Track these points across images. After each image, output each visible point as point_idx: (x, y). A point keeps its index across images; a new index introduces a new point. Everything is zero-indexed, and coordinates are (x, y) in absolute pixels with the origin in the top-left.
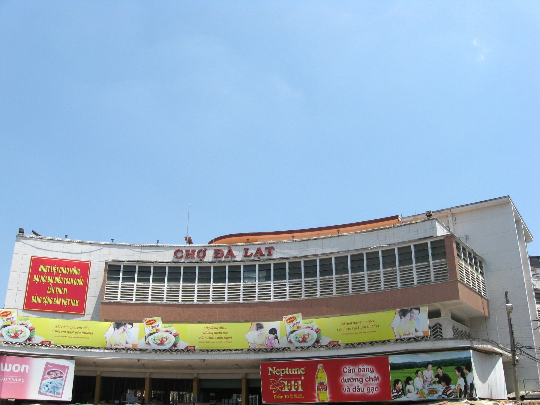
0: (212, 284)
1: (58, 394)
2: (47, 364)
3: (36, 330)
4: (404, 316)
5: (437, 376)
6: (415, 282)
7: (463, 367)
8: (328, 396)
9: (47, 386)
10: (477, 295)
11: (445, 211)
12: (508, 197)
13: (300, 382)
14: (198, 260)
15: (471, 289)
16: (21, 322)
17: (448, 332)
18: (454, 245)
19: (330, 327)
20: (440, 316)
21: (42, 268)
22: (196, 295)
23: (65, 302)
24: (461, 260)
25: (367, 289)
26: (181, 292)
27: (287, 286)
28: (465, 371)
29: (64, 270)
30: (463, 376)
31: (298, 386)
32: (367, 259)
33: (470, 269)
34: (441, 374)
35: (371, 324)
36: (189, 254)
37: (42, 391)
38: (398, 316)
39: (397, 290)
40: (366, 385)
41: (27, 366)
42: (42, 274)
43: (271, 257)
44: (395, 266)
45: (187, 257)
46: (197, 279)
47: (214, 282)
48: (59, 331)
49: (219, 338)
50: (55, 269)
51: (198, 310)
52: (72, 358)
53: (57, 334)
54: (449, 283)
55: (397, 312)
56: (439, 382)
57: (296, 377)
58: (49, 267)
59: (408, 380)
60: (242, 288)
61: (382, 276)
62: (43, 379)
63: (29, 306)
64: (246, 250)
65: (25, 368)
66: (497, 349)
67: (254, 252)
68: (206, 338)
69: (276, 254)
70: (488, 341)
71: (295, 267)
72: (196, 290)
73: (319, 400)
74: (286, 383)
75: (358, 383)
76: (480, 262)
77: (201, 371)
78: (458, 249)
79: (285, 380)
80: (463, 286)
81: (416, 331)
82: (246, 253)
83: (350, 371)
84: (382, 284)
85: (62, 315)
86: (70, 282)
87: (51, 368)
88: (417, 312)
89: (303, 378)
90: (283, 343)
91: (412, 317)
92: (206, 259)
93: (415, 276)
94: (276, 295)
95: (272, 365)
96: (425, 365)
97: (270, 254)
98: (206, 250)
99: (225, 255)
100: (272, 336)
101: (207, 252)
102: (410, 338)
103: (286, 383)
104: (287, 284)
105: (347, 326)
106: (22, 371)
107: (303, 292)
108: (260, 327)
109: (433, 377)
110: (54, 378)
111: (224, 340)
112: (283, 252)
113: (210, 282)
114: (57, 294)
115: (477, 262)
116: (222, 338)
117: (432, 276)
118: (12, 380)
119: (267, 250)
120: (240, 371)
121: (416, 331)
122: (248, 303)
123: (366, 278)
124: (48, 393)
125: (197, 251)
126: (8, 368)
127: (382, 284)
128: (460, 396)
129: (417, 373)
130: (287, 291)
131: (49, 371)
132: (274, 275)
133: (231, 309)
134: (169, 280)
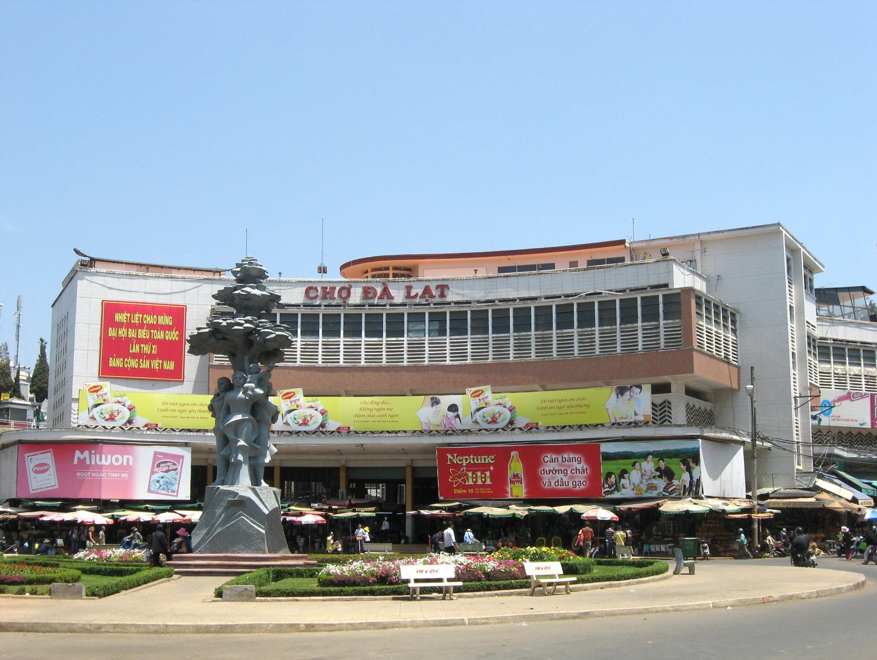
0: (363, 338)
1: (173, 492)
2: (156, 453)
3: (137, 409)
4: (622, 395)
5: (658, 469)
6: (640, 347)
7: (690, 460)
8: (524, 491)
9: (158, 482)
10: (721, 364)
11: (692, 238)
12: (779, 224)
13: (488, 473)
14: (340, 301)
15: (713, 357)
16: (116, 399)
17: (679, 414)
18: (693, 302)
19: (528, 405)
20: (670, 392)
21: (120, 317)
22: (342, 353)
23: (156, 364)
24: (702, 319)
25: (576, 352)
26: (320, 350)
27: (469, 344)
28: (691, 464)
29: (150, 319)
30: (689, 469)
31: (485, 477)
32: (578, 312)
33: (714, 329)
34: (663, 467)
35: (580, 403)
36: (327, 293)
37: (152, 489)
38: (614, 395)
39: (616, 356)
40: (571, 478)
41: (130, 457)
42: (120, 325)
43: (444, 300)
44: (616, 324)
45: (324, 297)
46: (342, 332)
47: (366, 336)
48: (166, 410)
49: (381, 416)
50: (137, 318)
51: (346, 374)
52: (186, 445)
53: (164, 413)
54: (682, 350)
55: (614, 390)
56: (660, 477)
57: (484, 467)
58: (129, 315)
59: (623, 473)
60: (405, 345)
61: (597, 336)
62: (153, 473)
63: (106, 372)
64: (409, 288)
65: (128, 460)
66: (735, 437)
67: (420, 291)
68: (363, 416)
69: (451, 297)
70: (723, 429)
71: (480, 318)
72: (342, 347)
73: (512, 495)
74: (470, 474)
75: (562, 476)
76: (733, 315)
77: (352, 457)
78: (698, 305)
79: (469, 471)
80: (700, 355)
81: (636, 414)
82: (409, 293)
83: (552, 461)
84: (597, 347)
85: (153, 383)
86: (159, 335)
87: (160, 458)
88: (638, 390)
89: (492, 468)
90: (466, 422)
91: (631, 397)
92: (351, 301)
93: (640, 339)
94: (454, 356)
95: (452, 452)
96: (644, 456)
97: (442, 295)
98: (351, 287)
99: (378, 295)
100: (451, 414)
101: (352, 290)
102: (631, 423)
103: (470, 474)
104: (469, 340)
105: (549, 405)
106: (125, 464)
107: (491, 353)
108: (435, 402)
109: (653, 471)
110: (167, 472)
111: (389, 419)
112: (461, 292)
113: (361, 336)
114: (144, 354)
115: (727, 316)
116: (385, 416)
117: (662, 341)
118: (113, 475)
119: (439, 290)
120: (404, 457)
121: (636, 414)
122: (415, 367)
123: (576, 338)
124: (160, 491)
125: (338, 289)
126: (106, 460)
127: (597, 347)
128: (684, 494)
129: (634, 464)
130: (469, 351)
131: (159, 462)
132: (451, 329)
133: (392, 373)
134: (304, 333)
